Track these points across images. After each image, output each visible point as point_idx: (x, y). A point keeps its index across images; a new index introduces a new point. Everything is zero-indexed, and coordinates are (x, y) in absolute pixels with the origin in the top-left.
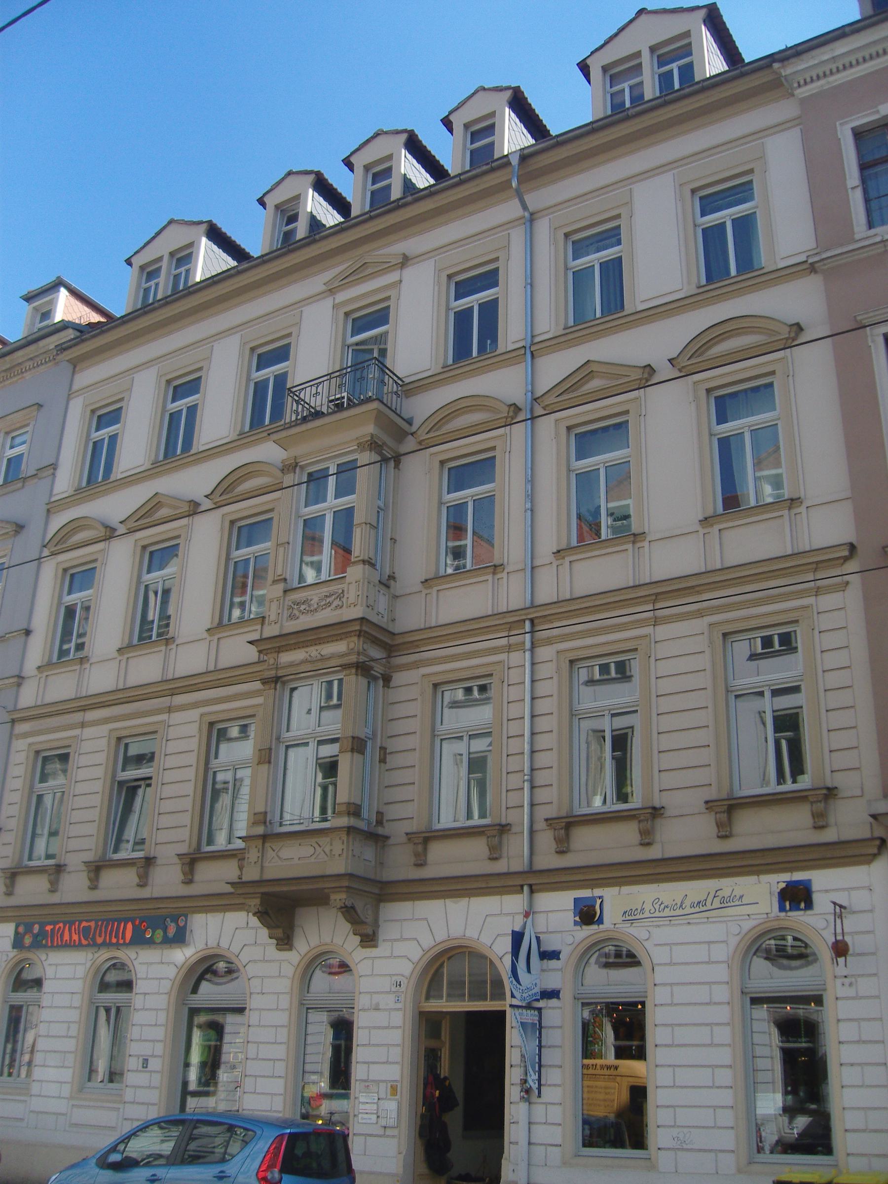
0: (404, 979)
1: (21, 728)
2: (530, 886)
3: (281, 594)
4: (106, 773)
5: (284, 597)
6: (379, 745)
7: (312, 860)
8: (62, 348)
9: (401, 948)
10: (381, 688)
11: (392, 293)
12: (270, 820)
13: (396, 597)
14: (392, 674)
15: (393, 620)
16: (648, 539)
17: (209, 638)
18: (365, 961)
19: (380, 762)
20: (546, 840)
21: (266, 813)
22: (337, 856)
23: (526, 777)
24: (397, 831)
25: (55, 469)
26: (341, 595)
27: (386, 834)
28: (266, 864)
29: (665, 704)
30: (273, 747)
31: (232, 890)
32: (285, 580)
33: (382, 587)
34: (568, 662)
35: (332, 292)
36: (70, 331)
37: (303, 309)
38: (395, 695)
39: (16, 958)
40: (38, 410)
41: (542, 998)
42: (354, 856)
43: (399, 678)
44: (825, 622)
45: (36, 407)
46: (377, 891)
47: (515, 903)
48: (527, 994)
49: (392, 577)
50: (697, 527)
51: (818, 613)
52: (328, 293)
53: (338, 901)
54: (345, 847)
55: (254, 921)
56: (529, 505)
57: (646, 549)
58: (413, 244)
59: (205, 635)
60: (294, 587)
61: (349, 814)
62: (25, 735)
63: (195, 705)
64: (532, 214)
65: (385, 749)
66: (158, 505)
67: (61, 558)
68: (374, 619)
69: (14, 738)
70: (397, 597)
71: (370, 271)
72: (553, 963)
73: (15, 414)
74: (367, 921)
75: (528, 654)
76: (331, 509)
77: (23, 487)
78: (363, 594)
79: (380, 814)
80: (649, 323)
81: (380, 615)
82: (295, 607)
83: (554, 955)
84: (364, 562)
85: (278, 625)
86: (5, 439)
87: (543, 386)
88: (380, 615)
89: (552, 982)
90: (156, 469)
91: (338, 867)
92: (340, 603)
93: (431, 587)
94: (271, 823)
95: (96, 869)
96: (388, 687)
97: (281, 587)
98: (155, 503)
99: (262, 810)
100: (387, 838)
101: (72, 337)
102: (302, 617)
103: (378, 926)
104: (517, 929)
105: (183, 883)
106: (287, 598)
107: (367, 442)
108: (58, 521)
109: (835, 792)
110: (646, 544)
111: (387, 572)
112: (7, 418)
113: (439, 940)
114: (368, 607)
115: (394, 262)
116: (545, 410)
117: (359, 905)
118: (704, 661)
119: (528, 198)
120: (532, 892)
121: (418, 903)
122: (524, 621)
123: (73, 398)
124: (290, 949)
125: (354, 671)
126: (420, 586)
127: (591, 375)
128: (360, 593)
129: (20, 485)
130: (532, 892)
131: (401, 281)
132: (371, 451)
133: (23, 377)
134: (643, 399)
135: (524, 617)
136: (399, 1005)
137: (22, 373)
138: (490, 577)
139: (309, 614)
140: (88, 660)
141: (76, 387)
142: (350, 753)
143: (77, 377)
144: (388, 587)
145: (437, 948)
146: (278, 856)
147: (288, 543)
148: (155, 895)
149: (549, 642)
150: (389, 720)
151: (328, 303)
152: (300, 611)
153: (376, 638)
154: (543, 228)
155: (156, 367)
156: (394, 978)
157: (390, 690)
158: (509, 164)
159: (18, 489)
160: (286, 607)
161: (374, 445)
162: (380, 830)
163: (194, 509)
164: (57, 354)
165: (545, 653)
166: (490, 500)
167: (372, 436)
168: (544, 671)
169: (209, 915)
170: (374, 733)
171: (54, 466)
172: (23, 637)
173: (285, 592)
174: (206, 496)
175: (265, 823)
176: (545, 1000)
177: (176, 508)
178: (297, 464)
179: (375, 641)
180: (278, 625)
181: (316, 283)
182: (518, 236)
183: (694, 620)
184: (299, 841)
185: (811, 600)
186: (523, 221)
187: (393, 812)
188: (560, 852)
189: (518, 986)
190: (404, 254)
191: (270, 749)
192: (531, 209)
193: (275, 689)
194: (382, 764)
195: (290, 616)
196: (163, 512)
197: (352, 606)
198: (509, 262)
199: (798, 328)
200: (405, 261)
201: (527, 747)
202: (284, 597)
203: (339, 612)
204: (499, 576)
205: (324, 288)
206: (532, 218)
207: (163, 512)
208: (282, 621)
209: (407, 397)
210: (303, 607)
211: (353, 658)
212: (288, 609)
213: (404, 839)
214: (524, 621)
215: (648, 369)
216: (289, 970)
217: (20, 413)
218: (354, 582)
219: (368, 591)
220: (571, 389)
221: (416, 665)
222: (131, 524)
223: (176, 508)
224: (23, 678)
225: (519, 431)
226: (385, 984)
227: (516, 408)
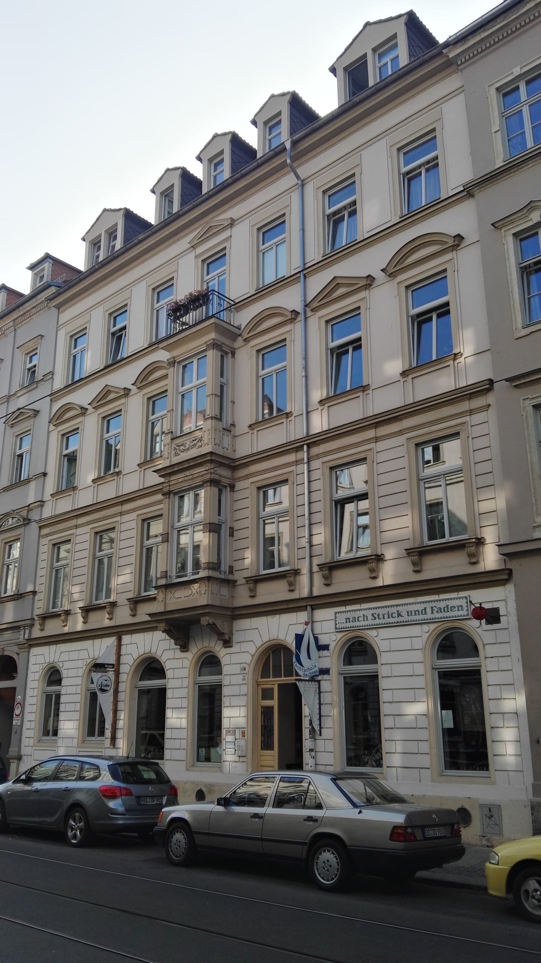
0: (247, 665)
1: (45, 531)
2: (311, 606)
3: (169, 441)
4: (89, 555)
5: (172, 443)
6: (228, 526)
7: (191, 597)
8: (51, 299)
9: (245, 647)
10: (229, 492)
11: (226, 244)
12: (170, 576)
13: (235, 437)
14: (235, 483)
15: (235, 451)
16: (371, 388)
17: (139, 470)
18: (226, 655)
19: (229, 536)
20: (318, 579)
21: (167, 571)
22: (203, 594)
23: (307, 540)
24: (239, 577)
25: (53, 374)
26: (200, 440)
27: (235, 579)
28: (168, 602)
29: (384, 491)
30: (170, 532)
31: (149, 619)
32: (172, 432)
33: (226, 431)
34: (328, 469)
35: (193, 247)
36: (53, 288)
37: (178, 261)
38: (238, 495)
39: (92, 662)
40: (42, 339)
41: (320, 674)
42: (213, 593)
43: (239, 485)
44: (477, 431)
45: (40, 337)
46: (230, 613)
47: (303, 616)
48: (308, 672)
49: (233, 425)
50: (400, 378)
51: (472, 426)
52: (192, 249)
53: (205, 621)
54: (207, 589)
55: (164, 635)
56: (304, 374)
57: (371, 394)
58: (234, 212)
59: (137, 468)
60: (178, 436)
61: (209, 569)
62: (47, 535)
63: (134, 510)
64: (303, 181)
65: (233, 528)
66: (109, 392)
67: (60, 428)
68: (220, 451)
69: (41, 538)
70: (236, 436)
71: (214, 231)
72: (325, 653)
73: (29, 343)
74: (225, 632)
75: (306, 466)
76: (195, 387)
77: (37, 387)
78: (212, 438)
79: (231, 568)
80: (364, 250)
81: (225, 449)
82: (178, 448)
83: (325, 647)
84: (212, 417)
85: (169, 460)
86: (25, 358)
87: (311, 296)
88: (225, 449)
89: (325, 663)
90: (108, 368)
91: (203, 601)
92: (200, 444)
93: (253, 429)
94: (170, 577)
95: (87, 610)
96: (233, 491)
97: (169, 437)
98: (106, 391)
99: (165, 570)
100: (236, 581)
101: (54, 291)
102: (181, 454)
103: (233, 634)
104: (300, 632)
105: (131, 615)
106: (173, 443)
107: (211, 343)
108: (57, 406)
109: (482, 540)
110: (370, 391)
111: (230, 422)
112: (25, 345)
113: (265, 641)
114: (216, 445)
115: (226, 223)
116: (312, 311)
117: (219, 623)
118: (404, 462)
119: (299, 171)
120: (313, 609)
121: (253, 619)
122: (303, 445)
123: (59, 330)
124: (187, 651)
125: (209, 484)
126: (247, 430)
127: (338, 286)
128: (210, 437)
129: (35, 386)
130: (313, 609)
131: (231, 236)
132: (213, 349)
133: (32, 319)
134: (368, 298)
135: (302, 443)
136: (244, 682)
137: (31, 316)
138: (284, 420)
139: (185, 452)
140: (77, 488)
141: (60, 323)
142: (208, 533)
143: (61, 316)
144: (230, 431)
145: (264, 645)
146: (173, 596)
147: (173, 410)
148: (117, 624)
149: (318, 457)
150: (235, 511)
151: (193, 254)
152: (180, 451)
153: (222, 463)
154: (310, 188)
155: (102, 306)
156: (242, 665)
157: (235, 493)
158: (285, 149)
159: (35, 388)
160: (173, 448)
161: (215, 345)
162: (230, 577)
163: (127, 392)
164: (48, 303)
165: (315, 464)
166: (284, 370)
167: (214, 339)
168: (316, 475)
169: (145, 633)
170: (226, 520)
171: (52, 373)
172: (42, 478)
173: (172, 439)
174: (133, 384)
175: (167, 577)
176: (322, 675)
177: (118, 393)
178: (175, 361)
179: (222, 465)
180: (169, 460)
181: (183, 243)
182: (295, 197)
183: (398, 437)
184: (185, 587)
185: (467, 419)
186: (297, 186)
187: (237, 566)
188: (327, 585)
189: (301, 667)
190: (231, 218)
191: (168, 533)
192: (302, 178)
193: (169, 498)
194: (231, 538)
195: (175, 454)
196: (112, 396)
197: (206, 445)
198: (291, 215)
199: (459, 238)
200: (232, 223)
201: (307, 522)
202: (172, 443)
203: (200, 449)
204: (290, 419)
205: (189, 246)
206: (303, 185)
207: (112, 396)
208: (171, 457)
209: (238, 312)
210: (181, 448)
211: (208, 477)
212: (174, 450)
213: (244, 581)
214: (303, 445)
215: (370, 278)
216: (187, 663)
217: (31, 342)
218: (207, 431)
219: (215, 435)
220: (327, 296)
221: (247, 477)
222: (95, 405)
223: (118, 393)
224: (44, 502)
225: (298, 326)
226: (237, 669)
227: (295, 313)
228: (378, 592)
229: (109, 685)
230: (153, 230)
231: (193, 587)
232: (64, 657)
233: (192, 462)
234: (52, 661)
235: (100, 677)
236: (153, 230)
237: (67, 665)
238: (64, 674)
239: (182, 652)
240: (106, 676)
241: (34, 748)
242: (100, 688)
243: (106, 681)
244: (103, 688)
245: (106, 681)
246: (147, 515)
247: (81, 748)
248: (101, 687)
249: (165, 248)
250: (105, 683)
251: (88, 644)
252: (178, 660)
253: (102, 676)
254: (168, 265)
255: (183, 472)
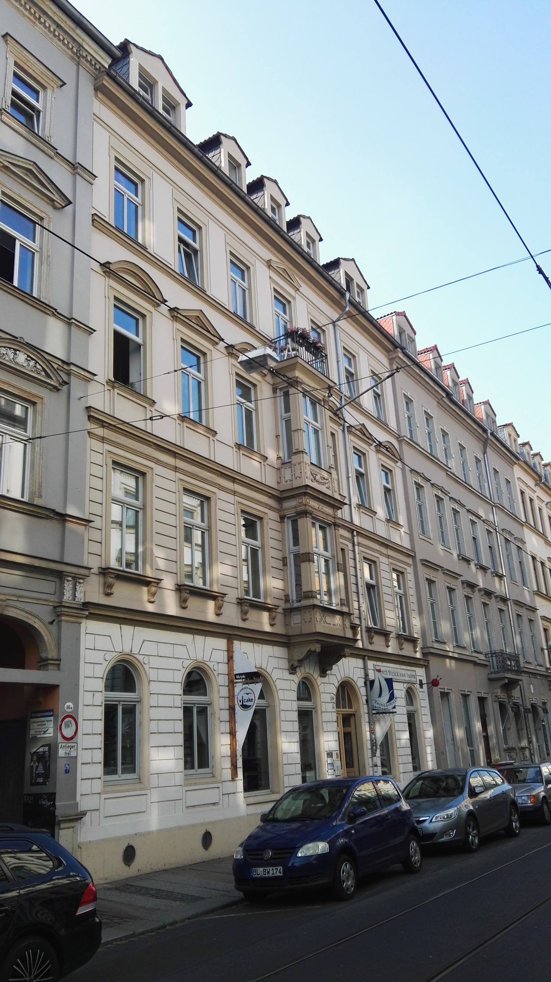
102: (315, 482)
228: (214, 628)
229: (252, 699)
230: (324, 273)
231: (317, 612)
232: (148, 649)
233: (338, 504)
234: (127, 650)
235: (240, 691)
236: (324, 273)
237: (155, 662)
238: (180, 676)
239: (290, 673)
240: (247, 688)
241: (103, 796)
242: (241, 704)
243: (248, 694)
244: (244, 703)
245: (248, 694)
246: (194, 488)
247: (191, 785)
248: (243, 703)
249: (244, 227)
250: (246, 697)
251: (186, 638)
252: (287, 682)
253: (242, 689)
254: (232, 237)
255: (319, 502)
